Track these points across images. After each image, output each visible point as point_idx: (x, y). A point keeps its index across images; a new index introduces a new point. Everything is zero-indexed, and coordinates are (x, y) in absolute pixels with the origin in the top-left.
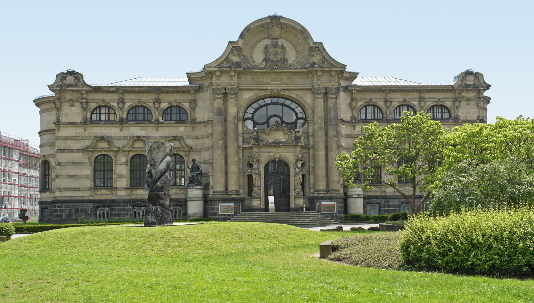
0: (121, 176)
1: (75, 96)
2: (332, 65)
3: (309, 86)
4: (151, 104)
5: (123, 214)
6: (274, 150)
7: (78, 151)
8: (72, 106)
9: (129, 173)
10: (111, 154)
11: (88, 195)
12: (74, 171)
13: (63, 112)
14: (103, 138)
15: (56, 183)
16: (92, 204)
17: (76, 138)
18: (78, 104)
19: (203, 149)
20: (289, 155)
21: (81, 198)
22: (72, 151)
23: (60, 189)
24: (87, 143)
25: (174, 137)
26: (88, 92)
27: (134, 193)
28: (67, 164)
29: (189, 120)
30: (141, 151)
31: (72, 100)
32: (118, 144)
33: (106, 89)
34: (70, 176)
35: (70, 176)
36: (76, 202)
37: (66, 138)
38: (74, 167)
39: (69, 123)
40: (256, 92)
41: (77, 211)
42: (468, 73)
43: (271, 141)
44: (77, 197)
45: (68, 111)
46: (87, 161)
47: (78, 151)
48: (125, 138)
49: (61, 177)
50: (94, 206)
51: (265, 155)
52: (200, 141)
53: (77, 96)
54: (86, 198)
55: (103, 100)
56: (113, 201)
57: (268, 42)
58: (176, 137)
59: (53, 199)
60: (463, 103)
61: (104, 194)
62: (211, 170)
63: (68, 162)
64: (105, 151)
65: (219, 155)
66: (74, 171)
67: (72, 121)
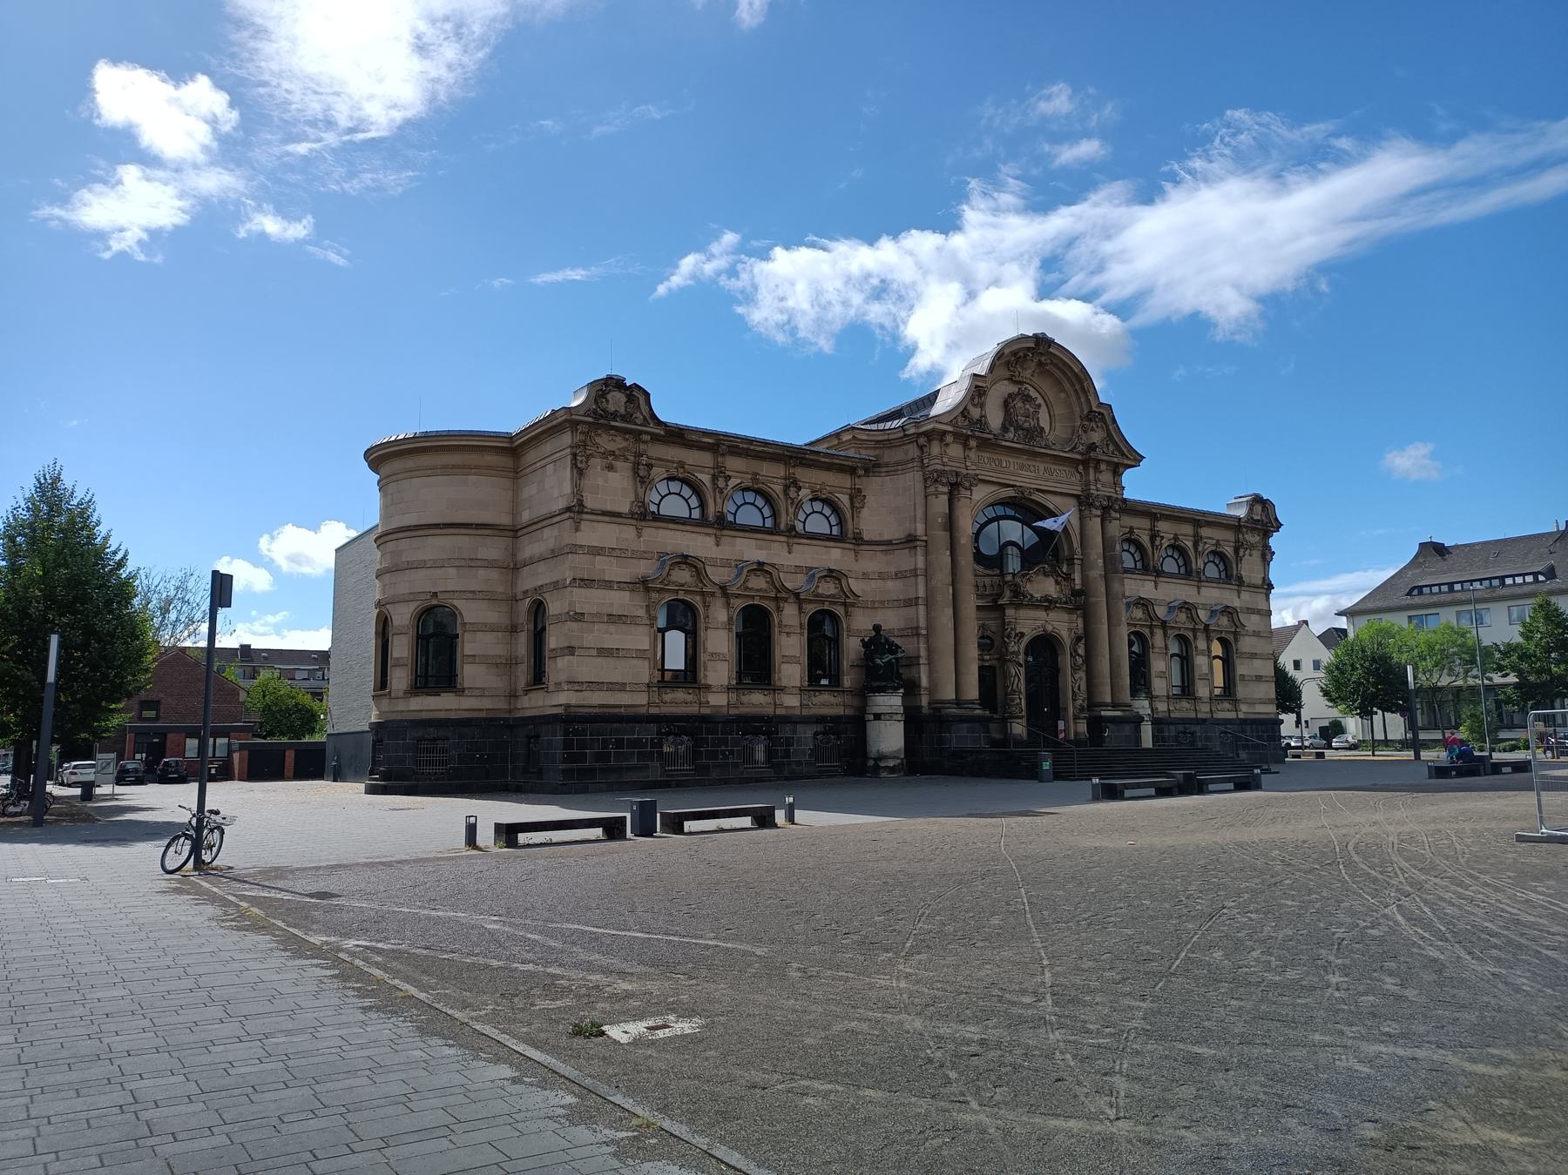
0: (788, 660)
1: (618, 444)
2: (1123, 454)
3: (1077, 490)
4: (778, 488)
5: (723, 752)
6: (1041, 614)
7: (621, 585)
8: (610, 468)
9: (734, 650)
10: (697, 600)
11: (644, 702)
12: (613, 638)
13: (587, 482)
14: (684, 560)
15: (558, 669)
16: (653, 727)
17: (617, 553)
18: (624, 468)
19: (882, 602)
20: (1062, 625)
21: (631, 711)
22: (608, 585)
23: (576, 685)
24: (644, 568)
25: (830, 570)
26: (655, 438)
27: (745, 699)
28: (597, 618)
29: (850, 535)
30: (686, 592)
31: (613, 453)
32: (717, 575)
33: (694, 437)
34: (604, 652)
35: (604, 652)
36: (620, 719)
37: (596, 551)
38: (612, 628)
39: (604, 513)
40: (994, 488)
41: (619, 743)
42: (613, 383)
43: (1037, 596)
44: (620, 706)
45: (600, 482)
46: (642, 612)
47: (621, 585)
48: (726, 563)
49: (582, 652)
50: (659, 733)
51: (1029, 623)
52: (873, 584)
53: (624, 444)
54: (643, 711)
55: (681, 464)
56: (704, 719)
57: (1014, 389)
58: (687, 557)
59: (560, 711)
60: (597, 462)
61: (757, 701)
62: (923, 653)
63: (599, 614)
64: (686, 592)
65: (945, 617)
66: (613, 638)
67: (609, 508)
